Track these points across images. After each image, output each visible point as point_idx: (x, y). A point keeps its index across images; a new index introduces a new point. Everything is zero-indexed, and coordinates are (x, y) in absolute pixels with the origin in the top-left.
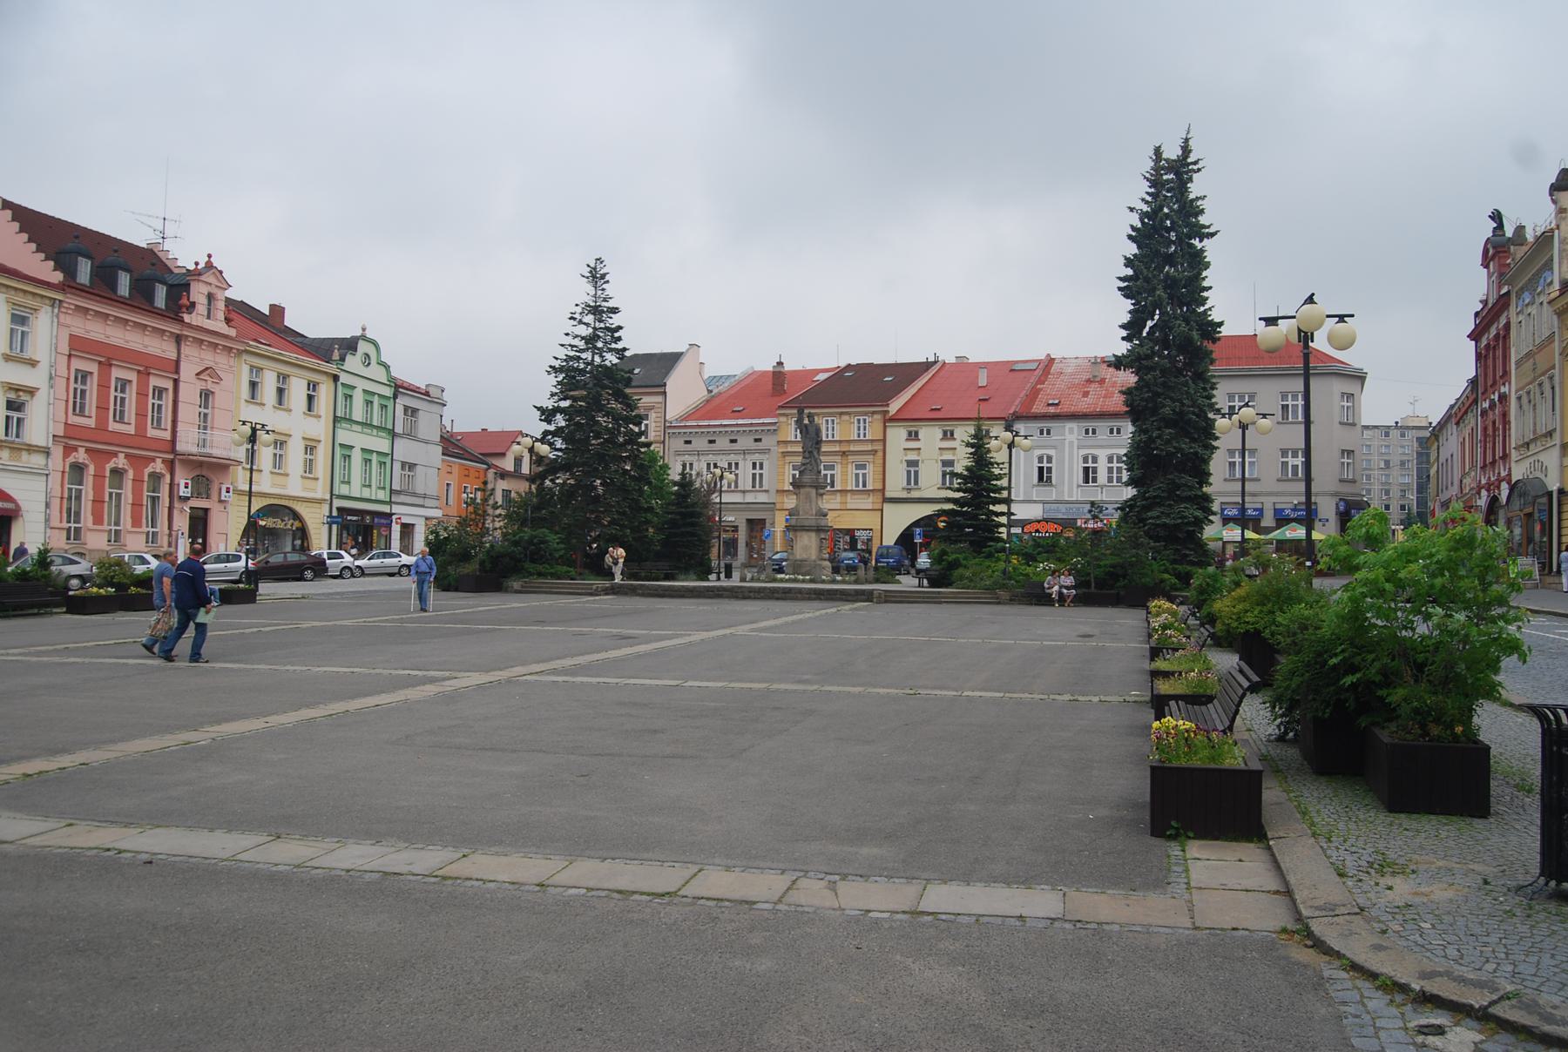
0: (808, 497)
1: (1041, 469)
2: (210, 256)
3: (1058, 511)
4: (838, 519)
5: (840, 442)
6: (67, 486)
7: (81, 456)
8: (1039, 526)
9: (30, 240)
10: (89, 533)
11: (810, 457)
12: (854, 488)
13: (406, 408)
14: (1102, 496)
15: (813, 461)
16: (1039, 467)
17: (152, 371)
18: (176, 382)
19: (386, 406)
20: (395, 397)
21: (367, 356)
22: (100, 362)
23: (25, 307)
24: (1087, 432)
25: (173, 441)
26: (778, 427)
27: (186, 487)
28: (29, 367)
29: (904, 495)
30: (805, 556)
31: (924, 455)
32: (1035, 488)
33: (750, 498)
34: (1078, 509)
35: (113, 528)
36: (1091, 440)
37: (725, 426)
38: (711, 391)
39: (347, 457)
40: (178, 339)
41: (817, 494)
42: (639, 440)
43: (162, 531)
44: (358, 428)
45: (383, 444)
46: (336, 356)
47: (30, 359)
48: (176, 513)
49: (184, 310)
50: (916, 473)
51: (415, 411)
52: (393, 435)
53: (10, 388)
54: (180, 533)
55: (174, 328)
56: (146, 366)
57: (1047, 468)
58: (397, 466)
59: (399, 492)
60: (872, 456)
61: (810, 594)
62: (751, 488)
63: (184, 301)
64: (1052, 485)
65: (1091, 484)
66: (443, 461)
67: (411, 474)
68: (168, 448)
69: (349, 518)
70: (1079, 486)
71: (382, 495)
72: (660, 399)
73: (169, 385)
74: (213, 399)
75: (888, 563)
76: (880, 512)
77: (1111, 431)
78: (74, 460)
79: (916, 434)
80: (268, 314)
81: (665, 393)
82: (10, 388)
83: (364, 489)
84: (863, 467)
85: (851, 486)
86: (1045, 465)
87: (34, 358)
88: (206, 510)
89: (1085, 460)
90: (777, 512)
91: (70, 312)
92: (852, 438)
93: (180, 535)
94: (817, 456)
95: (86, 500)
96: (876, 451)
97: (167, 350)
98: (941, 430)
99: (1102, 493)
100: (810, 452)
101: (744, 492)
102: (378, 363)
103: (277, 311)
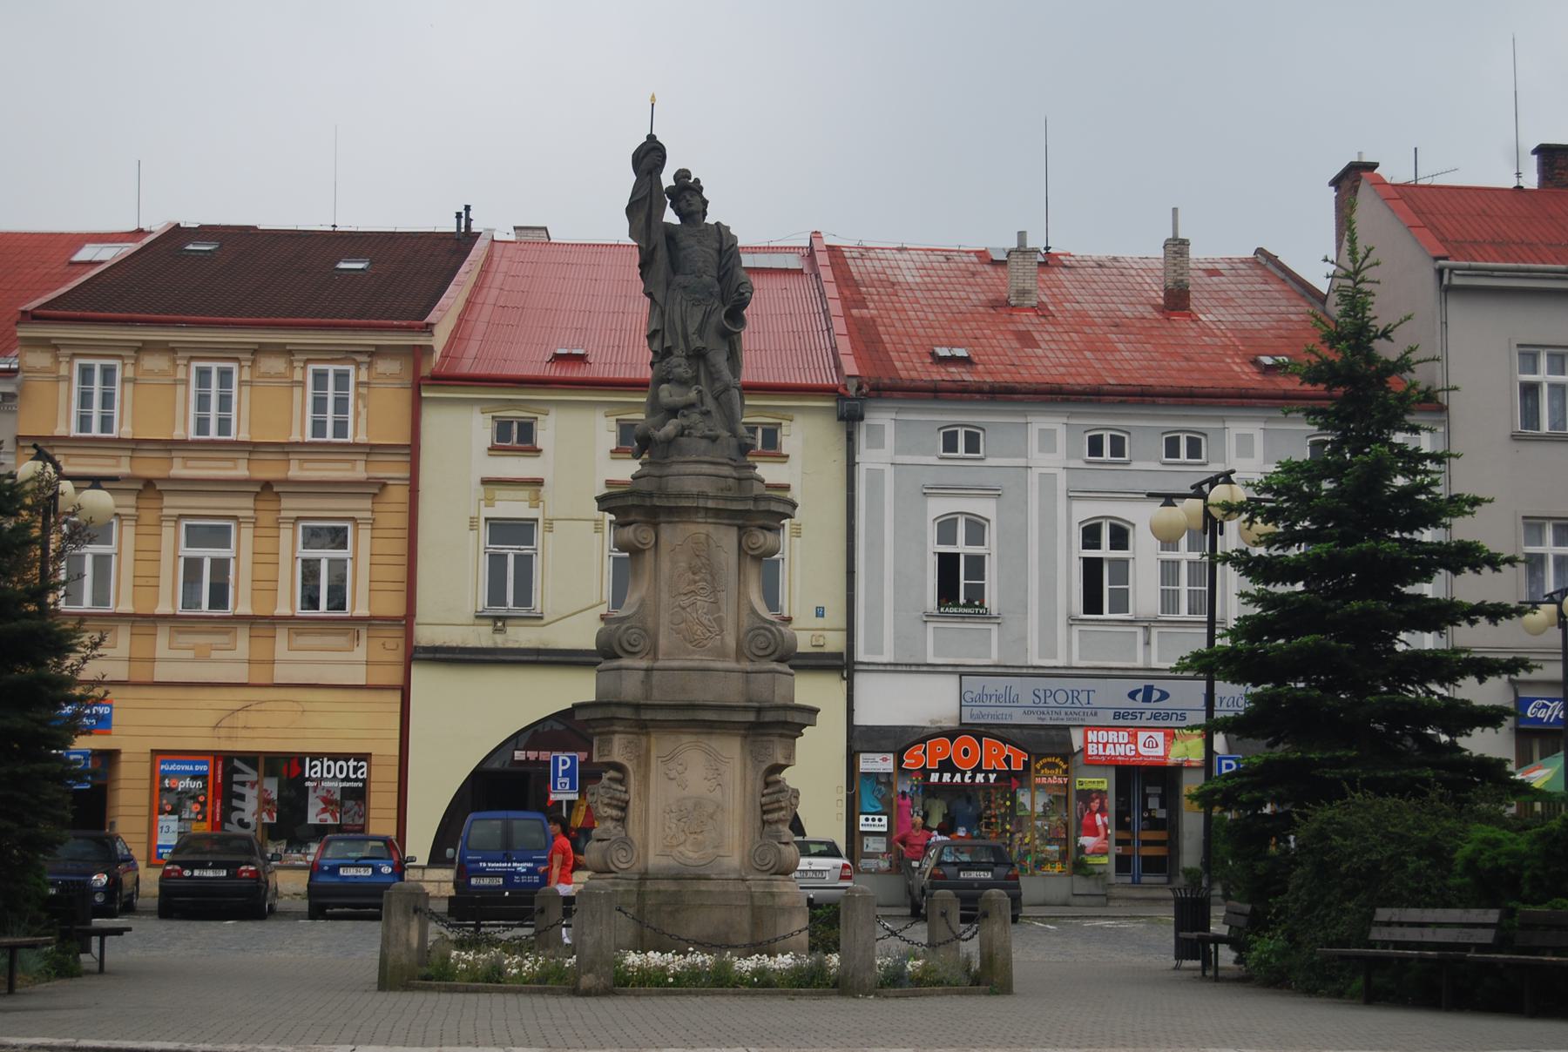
0: (703, 567)
1: (948, 564)
3: (1009, 700)
4: (242, 717)
5: (135, 445)
8: (949, 750)
12: (299, 612)
14: (1147, 655)
15: (710, 404)
16: (1087, 561)
24: (1095, 446)
26: (22, 387)
29: (482, 637)
30: (690, 854)
31: (554, 502)
32: (930, 626)
34: (1074, 695)
36: (961, 466)
50: (524, 564)
57: (967, 557)
60: (367, 503)
64: (986, 617)
65: (1106, 615)
70: (1072, 621)
75: (508, 876)
76: (396, 698)
77: (950, 443)
79: (527, 431)
84: (219, 536)
85: (168, 602)
86: (961, 547)
89: (1091, 535)
92: (295, 437)
96: (383, 485)
98: (612, 423)
99: (1147, 643)
100: (698, 356)
102: (545, 229)
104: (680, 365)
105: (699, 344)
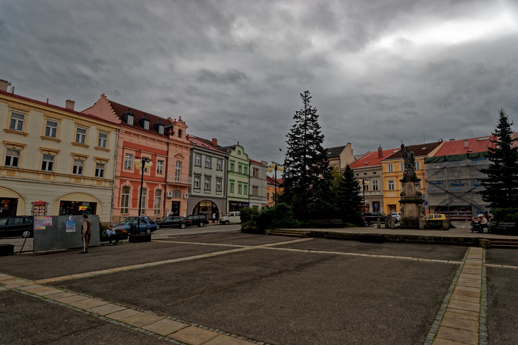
0: (410, 187)
2: (180, 117)
6: (121, 194)
7: (128, 183)
9: (116, 114)
10: (130, 211)
11: (409, 167)
13: (254, 168)
15: (411, 170)
17: (157, 154)
18: (167, 158)
19: (247, 168)
20: (250, 165)
21: (239, 151)
22: (152, 154)
23: (105, 131)
25: (166, 178)
27: (170, 194)
28: (56, 143)
33: (373, 194)
35: (124, 208)
37: (362, 169)
38: (356, 159)
39: (232, 184)
40: (168, 144)
41: (415, 185)
42: (320, 153)
43: (161, 209)
44: (237, 175)
45: (246, 180)
46: (228, 151)
47: (107, 149)
48: (167, 203)
49: (170, 134)
51: (257, 170)
52: (249, 177)
53: (75, 155)
54: (168, 210)
55: (166, 140)
56: (155, 153)
58: (251, 187)
59: (252, 196)
61: (431, 240)
62: (373, 190)
63: (170, 131)
66: (268, 186)
67: (257, 190)
68: (164, 180)
69: (233, 204)
71: (245, 197)
72: (338, 161)
73: (164, 159)
74: (182, 164)
78: (125, 185)
80: (212, 141)
81: (340, 159)
82: (97, 159)
83: (239, 194)
87: (108, 149)
88: (179, 202)
90: (384, 199)
91: (124, 133)
93: (168, 211)
94: (413, 167)
95: (130, 199)
97: (164, 148)
100: (409, 165)
101: (370, 192)
103: (215, 140)
104: (407, 167)
105: (409, 164)
